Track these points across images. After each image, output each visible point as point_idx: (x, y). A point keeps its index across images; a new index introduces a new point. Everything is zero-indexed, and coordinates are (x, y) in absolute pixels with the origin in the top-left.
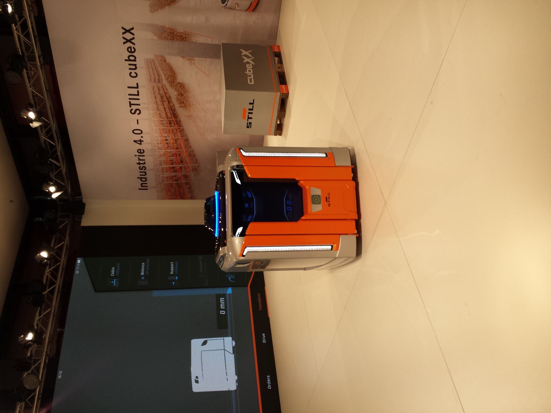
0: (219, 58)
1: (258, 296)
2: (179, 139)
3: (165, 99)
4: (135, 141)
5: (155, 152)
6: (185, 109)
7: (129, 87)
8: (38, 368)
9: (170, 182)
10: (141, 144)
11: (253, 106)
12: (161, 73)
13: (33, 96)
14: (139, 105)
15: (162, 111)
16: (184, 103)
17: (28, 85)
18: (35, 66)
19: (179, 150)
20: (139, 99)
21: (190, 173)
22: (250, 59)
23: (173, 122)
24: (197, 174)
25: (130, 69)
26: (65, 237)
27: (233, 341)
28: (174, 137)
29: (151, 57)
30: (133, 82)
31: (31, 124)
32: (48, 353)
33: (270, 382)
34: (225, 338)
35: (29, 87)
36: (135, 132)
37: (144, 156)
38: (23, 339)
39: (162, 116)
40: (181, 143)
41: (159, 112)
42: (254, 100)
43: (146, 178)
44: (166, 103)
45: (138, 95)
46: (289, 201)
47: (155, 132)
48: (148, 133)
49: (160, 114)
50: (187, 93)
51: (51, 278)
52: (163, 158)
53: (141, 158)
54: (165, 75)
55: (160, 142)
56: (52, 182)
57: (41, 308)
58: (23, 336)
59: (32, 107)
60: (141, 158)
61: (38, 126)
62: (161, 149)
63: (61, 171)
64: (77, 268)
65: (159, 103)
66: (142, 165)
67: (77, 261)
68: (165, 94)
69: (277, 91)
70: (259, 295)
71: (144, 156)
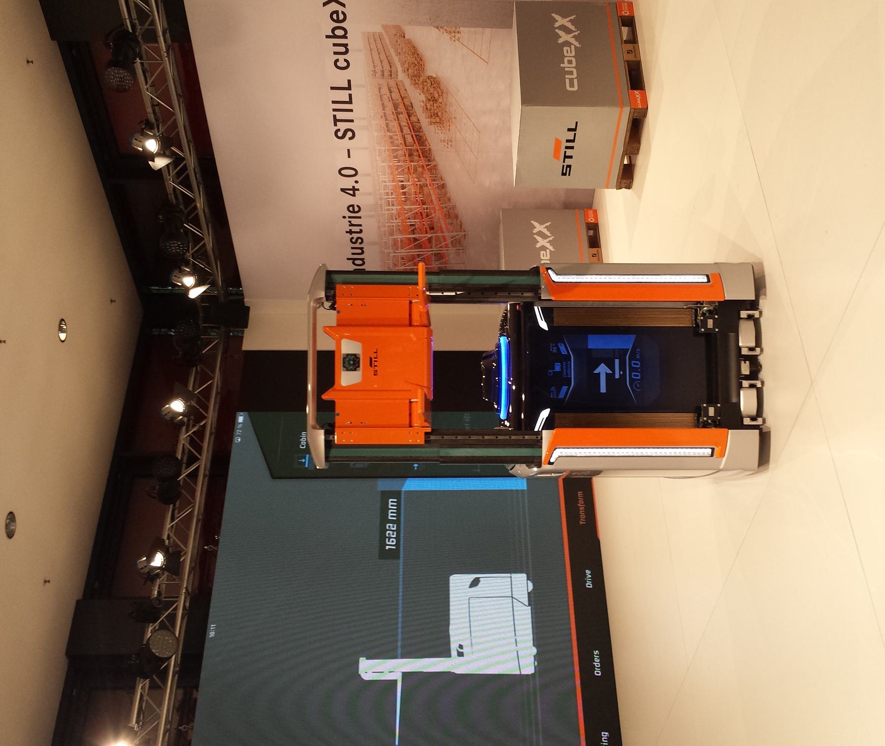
0: (510, 27)
1: (578, 497)
2: (427, 184)
3: (401, 108)
4: (343, 190)
5: (382, 211)
6: (439, 128)
7: (332, 88)
8: (172, 618)
9: (408, 266)
10: (354, 195)
11: (575, 134)
12: (396, 59)
13: (153, 106)
14: (352, 121)
15: (395, 132)
16: (438, 116)
17: (144, 86)
18: (158, 51)
19: (427, 206)
20: (351, 111)
21: (447, 250)
22: (572, 35)
23: (416, 153)
24: (461, 251)
25: (335, 53)
26: (213, 372)
27: (528, 581)
28: (419, 181)
29: (378, 29)
30: (341, 78)
31: (150, 163)
32: (190, 590)
33: (599, 664)
34: (514, 575)
35: (146, 90)
36: (343, 172)
37: (360, 217)
38: (145, 564)
39: (396, 142)
40: (432, 193)
41: (389, 134)
42: (577, 123)
43: (362, 260)
44: (403, 117)
45: (350, 102)
46: (636, 362)
47: (382, 172)
48: (374, 244)
49: (391, 138)
50: (445, 98)
51: (190, 448)
52: (396, 222)
53: (354, 221)
54: (403, 64)
55: (390, 191)
56: (151, 132)
57: (174, 505)
58: (145, 559)
59: (150, 127)
60: (354, 221)
61: (164, 167)
62: (393, 205)
63: (204, 245)
64: (238, 432)
65: (391, 117)
66: (355, 236)
67: (238, 418)
68: (403, 99)
69: (622, 105)
70: (580, 494)
71: (360, 217)
